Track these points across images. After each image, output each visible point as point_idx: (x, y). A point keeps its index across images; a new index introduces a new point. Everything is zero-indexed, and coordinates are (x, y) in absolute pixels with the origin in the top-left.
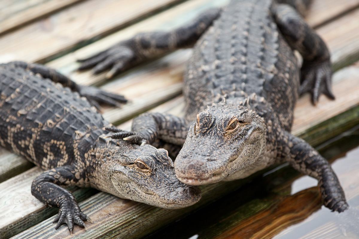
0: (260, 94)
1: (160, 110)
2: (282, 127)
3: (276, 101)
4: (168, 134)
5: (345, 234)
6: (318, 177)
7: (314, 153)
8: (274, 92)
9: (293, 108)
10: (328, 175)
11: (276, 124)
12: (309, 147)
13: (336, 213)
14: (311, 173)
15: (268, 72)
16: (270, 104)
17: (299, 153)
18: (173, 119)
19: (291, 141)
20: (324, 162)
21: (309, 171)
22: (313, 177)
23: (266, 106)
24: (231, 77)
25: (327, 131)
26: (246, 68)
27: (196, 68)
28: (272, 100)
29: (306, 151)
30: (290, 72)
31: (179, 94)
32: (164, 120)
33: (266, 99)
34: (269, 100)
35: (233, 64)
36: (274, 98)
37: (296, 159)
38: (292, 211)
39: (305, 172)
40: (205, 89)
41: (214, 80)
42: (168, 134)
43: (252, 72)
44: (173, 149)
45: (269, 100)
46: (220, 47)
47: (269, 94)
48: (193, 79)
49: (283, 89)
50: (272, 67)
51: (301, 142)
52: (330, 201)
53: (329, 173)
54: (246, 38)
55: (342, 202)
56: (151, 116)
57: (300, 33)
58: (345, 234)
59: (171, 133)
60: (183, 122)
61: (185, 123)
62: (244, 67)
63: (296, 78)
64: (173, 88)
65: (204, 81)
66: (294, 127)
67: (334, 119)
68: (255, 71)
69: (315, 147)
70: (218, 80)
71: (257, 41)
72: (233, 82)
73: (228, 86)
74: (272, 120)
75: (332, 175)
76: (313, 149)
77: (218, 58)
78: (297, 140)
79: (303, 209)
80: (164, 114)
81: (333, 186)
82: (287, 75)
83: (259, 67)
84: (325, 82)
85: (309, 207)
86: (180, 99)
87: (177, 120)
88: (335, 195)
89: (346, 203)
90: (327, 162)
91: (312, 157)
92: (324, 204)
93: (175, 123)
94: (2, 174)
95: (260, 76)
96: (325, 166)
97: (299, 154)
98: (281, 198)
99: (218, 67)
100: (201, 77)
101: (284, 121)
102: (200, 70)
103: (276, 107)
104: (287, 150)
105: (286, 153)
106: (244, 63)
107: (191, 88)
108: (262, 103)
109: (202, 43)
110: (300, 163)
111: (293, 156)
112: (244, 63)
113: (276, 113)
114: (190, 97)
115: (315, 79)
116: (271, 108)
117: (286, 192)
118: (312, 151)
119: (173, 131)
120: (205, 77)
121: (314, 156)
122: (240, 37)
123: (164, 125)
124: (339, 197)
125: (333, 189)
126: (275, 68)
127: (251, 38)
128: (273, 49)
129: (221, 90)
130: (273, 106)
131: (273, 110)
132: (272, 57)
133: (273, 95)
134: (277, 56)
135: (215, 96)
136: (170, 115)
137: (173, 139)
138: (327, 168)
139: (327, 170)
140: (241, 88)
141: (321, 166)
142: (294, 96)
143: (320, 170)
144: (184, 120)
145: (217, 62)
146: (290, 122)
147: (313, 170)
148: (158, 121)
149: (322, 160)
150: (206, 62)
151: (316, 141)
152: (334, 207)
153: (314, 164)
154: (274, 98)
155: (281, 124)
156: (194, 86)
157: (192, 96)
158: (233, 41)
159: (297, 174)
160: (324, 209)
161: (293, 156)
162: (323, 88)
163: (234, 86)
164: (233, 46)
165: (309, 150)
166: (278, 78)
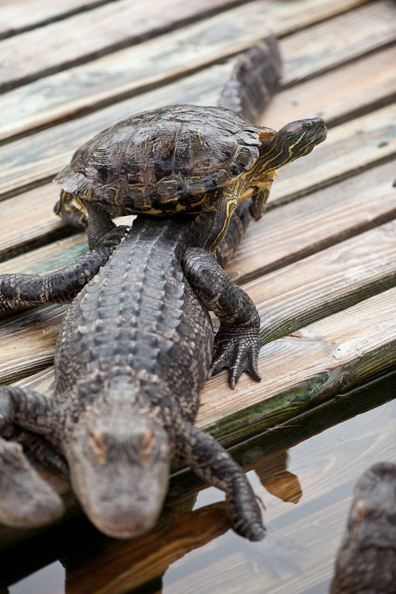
0: (152, 371)
1: (22, 385)
2: (183, 416)
3: (175, 379)
4: (27, 419)
5: (256, 570)
6: (227, 489)
7: (224, 455)
8: (172, 367)
9: (199, 390)
10: (240, 487)
11: (174, 413)
12: (218, 446)
13: (246, 541)
14: (218, 483)
15: (166, 338)
16: (166, 384)
17: (204, 454)
18: (37, 398)
19: (195, 436)
20: (236, 468)
21: (215, 480)
22: (221, 488)
23: (161, 387)
24: (115, 345)
25: (246, 425)
26: (137, 333)
27: (71, 329)
28: (170, 378)
29: (213, 451)
30: (198, 340)
31: (47, 364)
32: (23, 399)
33: (160, 377)
34: (165, 378)
35: (119, 325)
36: (173, 375)
37: (199, 461)
38: (189, 534)
39: (210, 481)
40: (79, 359)
41: (92, 348)
42: (27, 419)
43: (144, 338)
44: (32, 440)
45: (165, 378)
46: (104, 301)
47: (165, 368)
48: (66, 343)
49: (186, 363)
50: (173, 332)
51: (208, 439)
52: (240, 522)
53: (242, 484)
54: (141, 291)
55: (256, 525)
56: (6, 392)
57: (217, 287)
58: (256, 570)
59: (32, 418)
60: (49, 404)
61: (52, 405)
62: (133, 330)
63: (207, 350)
64: (42, 355)
65: (78, 347)
66: (199, 417)
67: (257, 407)
68: (149, 337)
69: (226, 447)
70: (97, 348)
71: (155, 294)
72: (116, 352)
73: (109, 358)
74: (170, 407)
75: (247, 487)
76: (223, 449)
77: (100, 316)
78: (203, 435)
79: (203, 532)
80: (25, 391)
81: (246, 501)
82: (193, 344)
83: (154, 332)
84: (249, 356)
85: (213, 529)
86: (50, 371)
87: (42, 400)
88: (248, 514)
89: (262, 526)
90: (241, 469)
91: (221, 461)
92: (232, 527)
93: (37, 405)
94: (250, 380)
95: (155, 344)
96: (237, 475)
97: (204, 456)
98: (176, 516)
99: (98, 329)
100: (78, 340)
101: (186, 407)
102: (76, 331)
103: (175, 388)
104: (188, 448)
105: (186, 453)
106: (135, 325)
107: (63, 356)
108: (155, 384)
109: (83, 295)
110: (204, 468)
111: (196, 457)
112: (135, 325)
113: (176, 396)
114: (60, 368)
115: (236, 351)
116: (168, 389)
117: (183, 507)
118: (222, 451)
119: (34, 416)
120: (81, 342)
121: (224, 459)
122: (132, 288)
123: (22, 406)
124: (253, 517)
125: (246, 506)
126: (176, 334)
127: (148, 291)
128: (176, 308)
129: (100, 363)
130: (170, 386)
131: (170, 392)
132: (173, 318)
133: (171, 370)
134: (181, 317)
135: (91, 372)
136: (33, 393)
137: (34, 426)
138: (239, 477)
139: (240, 479)
140: (126, 360)
141: (232, 473)
142: (201, 373)
143: (229, 479)
144: (52, 402)
145: (99, 322)
146: (194, 408)
147: (221, 479)
148: (16, 401)
149: (234, 466)
150: (84, 321)
151: (230, 438)
152: (245, 532)
153: (223, 470)
154: (173, 375)
155: (181, 412)
156: (65, 353)
157: (62, 367)
158: (123, 294)
159: (202, 484)
160: (230, 534)
161: (196, 457)
162: (245, 364)
163: (118, 358)
164: (122, 300)
165: (217, 451)
166: (180, 348)
